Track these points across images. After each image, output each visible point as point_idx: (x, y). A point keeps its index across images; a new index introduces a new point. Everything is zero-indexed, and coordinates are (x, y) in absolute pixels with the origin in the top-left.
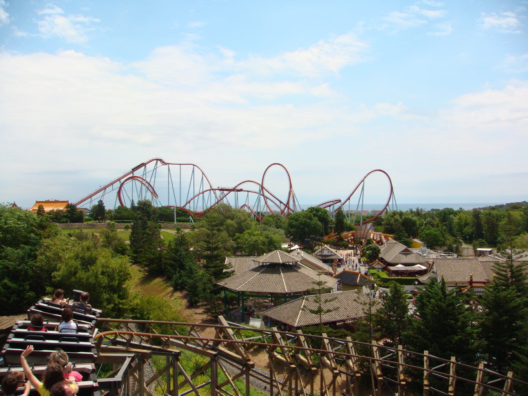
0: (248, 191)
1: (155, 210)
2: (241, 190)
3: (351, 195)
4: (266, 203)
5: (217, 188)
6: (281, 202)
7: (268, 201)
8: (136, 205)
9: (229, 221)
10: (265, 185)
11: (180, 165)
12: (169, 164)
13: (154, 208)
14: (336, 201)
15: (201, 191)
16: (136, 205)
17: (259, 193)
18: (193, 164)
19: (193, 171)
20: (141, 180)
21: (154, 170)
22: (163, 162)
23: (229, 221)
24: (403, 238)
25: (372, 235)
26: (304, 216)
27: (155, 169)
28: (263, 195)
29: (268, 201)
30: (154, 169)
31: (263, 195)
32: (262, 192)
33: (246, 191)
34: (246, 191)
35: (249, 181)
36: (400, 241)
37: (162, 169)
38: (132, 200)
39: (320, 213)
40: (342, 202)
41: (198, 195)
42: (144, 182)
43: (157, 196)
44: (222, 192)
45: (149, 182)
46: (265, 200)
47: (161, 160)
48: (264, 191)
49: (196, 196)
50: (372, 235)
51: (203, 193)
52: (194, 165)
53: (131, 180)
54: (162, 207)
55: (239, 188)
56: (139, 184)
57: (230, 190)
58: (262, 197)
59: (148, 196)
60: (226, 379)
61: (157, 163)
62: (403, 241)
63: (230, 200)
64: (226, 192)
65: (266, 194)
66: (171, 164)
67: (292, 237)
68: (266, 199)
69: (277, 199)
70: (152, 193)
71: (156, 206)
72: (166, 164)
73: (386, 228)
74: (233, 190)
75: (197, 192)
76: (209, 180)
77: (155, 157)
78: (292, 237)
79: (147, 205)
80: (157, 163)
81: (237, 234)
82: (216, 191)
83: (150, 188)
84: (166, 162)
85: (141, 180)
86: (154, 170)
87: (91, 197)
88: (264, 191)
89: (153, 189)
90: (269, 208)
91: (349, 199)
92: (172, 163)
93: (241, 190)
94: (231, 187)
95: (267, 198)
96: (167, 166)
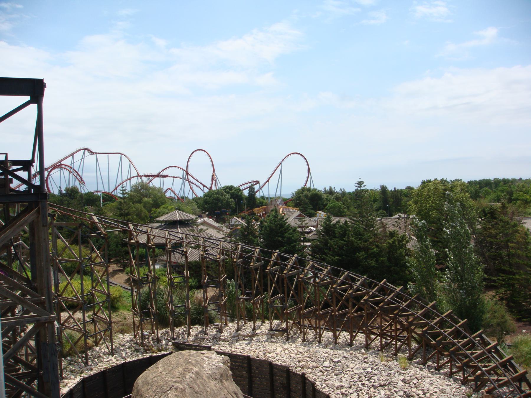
0: (174, 177)
1: (81, 196)
2: (167, 176)
3: (271, 177)
4: (191, 188)
5: (143, 175)
6: (204, 186)
7: (194, 186)
8: (64, 192)
9: (146, 199)
10: (189, 171)
11: (108, 154)
12: (96, 153)
13: (81, 193)
14: (254, 182)
15: (129, 177)
16: (64, 192)
17: (184, 179)
18: (120, 152)
19: (121, 160)
20: (69, 169)
21: (82, 159)
22: (91, 152)
23: (146, 199)
24: (308, 210)
25: (281, 209)
26: (216, 193)
27: (83, 158)
28: (188, 180)
29: (194, 186)
30: (82, 158)
31: (188, 180)
32: (187, 178)
33: (171, 177)
34: (171, 177)
35: (172, 166)
36: (305, 213)
37: (90, 159)
38: (60, 187)
39: (233, 191)
40: (261, 184)
41: (127, 181)
42: (72, 171)
43: (84, 183)
44: (148, 178)
45: (77, 171)
46: (190, 185)
47: (88, 150)
48: (189, 176)
49: (124, 182)
50: (281, 209)
51: (130, 179)
52: (121, 154)
53: (58, 169)
54: (89, 192)
55: (163, 173)
56: (66, 173)
57: (154, 176)
58: (187, 182)
59: (77, 184)
60: (64, 245)
61: (84, 152)
62: (308, 212)
63: (156, 183)
64: (151, 178)
65: (191, 179)
66: (99, 153)
67: (207, 213)
68: (190, 183)
69: (200, 183)
70: (79, 180)
71: (83, 192)
72: (94, 153)
73: (296, 203)
74: (158, 176)
75: (125, 178)
76: (137, 168)
77: (82, 147)
78: (207, 213)
79: (75, 191)
80: (84, 152)
81: (154, 209)
82: (142, 177)
83: (78, 177)
84: (94, 151)
85: (69, 169)
86: (82, 159)
87: (19, 187)
88: (189, 176)
89: (81, 178)
90: (194, 194)
91: (268, 181)
92: (99, 152)
93: (167, 176)
94: (155, 173)
95: (192, 183)
96: (95, 155)
